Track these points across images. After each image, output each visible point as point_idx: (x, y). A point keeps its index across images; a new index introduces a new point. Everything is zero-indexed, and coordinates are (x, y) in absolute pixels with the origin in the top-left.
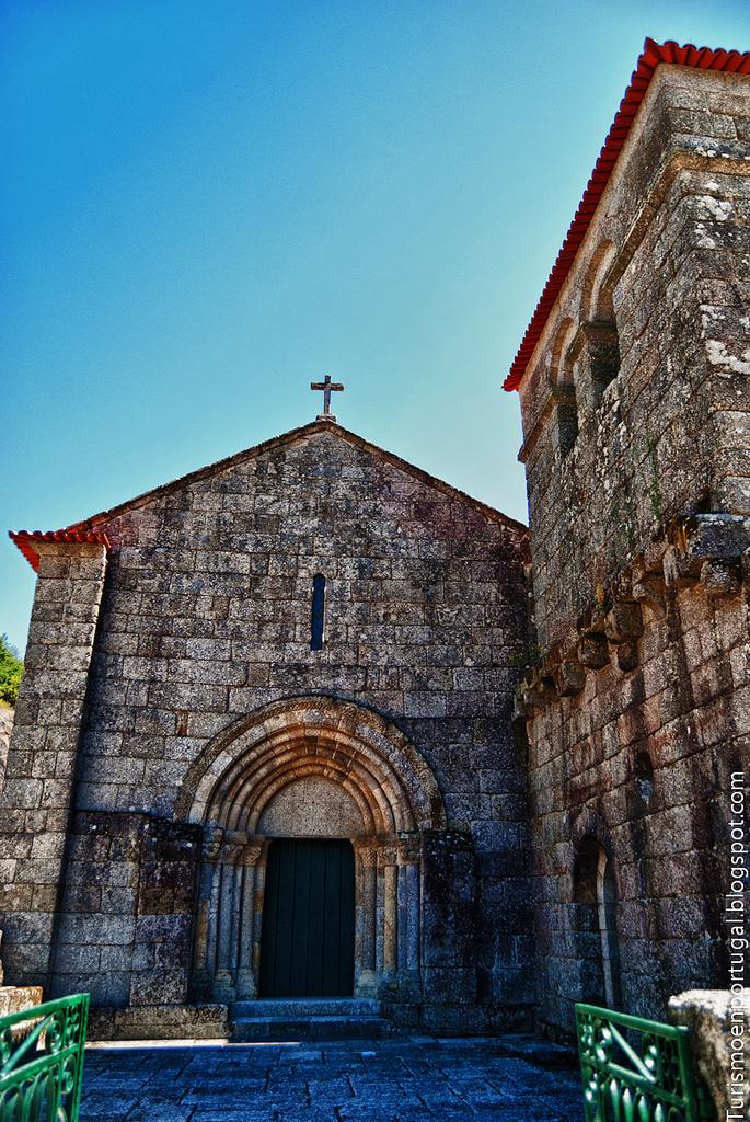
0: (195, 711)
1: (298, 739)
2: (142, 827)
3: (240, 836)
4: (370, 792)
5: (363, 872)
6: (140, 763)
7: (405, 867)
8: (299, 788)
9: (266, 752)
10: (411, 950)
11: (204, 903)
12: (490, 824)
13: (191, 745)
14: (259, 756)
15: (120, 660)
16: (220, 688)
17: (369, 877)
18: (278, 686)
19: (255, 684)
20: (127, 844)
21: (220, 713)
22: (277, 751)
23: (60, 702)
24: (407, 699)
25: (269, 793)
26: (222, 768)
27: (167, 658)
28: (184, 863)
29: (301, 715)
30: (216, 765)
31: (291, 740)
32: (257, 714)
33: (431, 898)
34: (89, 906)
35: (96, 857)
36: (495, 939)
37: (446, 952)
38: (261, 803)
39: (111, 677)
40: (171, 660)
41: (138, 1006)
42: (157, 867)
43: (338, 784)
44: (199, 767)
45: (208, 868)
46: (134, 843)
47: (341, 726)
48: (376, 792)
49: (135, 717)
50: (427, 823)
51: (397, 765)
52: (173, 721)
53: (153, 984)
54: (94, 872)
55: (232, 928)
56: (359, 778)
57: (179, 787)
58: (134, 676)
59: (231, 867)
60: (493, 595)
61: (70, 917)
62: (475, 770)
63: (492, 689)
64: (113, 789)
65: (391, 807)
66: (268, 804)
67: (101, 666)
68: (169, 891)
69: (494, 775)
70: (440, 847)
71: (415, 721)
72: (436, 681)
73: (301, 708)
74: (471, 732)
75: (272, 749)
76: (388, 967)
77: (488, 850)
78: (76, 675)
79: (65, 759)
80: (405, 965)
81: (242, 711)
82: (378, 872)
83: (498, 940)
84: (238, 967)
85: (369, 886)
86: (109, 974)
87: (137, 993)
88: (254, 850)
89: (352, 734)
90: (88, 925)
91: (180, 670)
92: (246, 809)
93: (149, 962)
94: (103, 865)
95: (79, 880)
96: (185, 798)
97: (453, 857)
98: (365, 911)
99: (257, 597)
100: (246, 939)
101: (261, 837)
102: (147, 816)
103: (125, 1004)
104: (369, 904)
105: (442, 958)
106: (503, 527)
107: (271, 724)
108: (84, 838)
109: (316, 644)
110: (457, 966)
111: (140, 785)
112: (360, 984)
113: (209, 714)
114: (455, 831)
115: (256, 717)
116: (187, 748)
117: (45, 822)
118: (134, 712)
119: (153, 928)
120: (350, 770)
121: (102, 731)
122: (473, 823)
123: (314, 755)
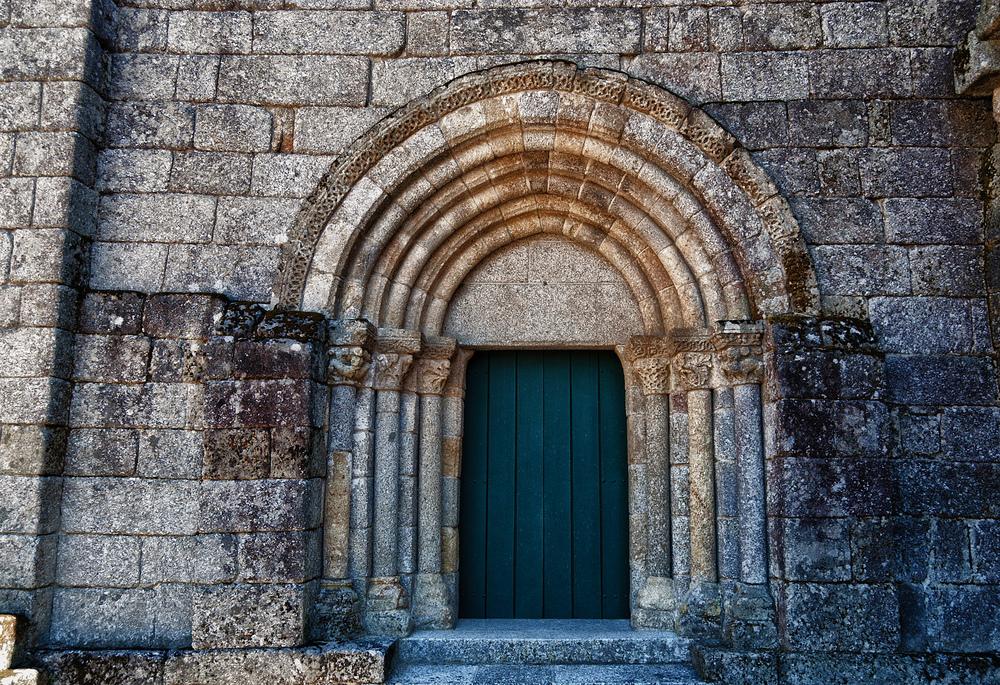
0: (308, 105)
1: (511, 155)
2: (208, 318)
3: (408, 339)
4: (654, 256)
5: (643, 404)
6: (206, 205)
8: (517, 257)
9: (448, 183)
10: (750, 546)
11: (339, 459)
12: (910, 303)
13: (303, 170)
14: (437, 191)
15: (162, 17)
16: (354, 61)
17: (655, 411)
18: (468, 53)
19: (422, 50)
20: (182, 351)
22: (472, 181)
23: (36, 85)
24: (728, 67)
25: (461, 265)
26: (363, 210)
27: (251, 10)
28: (287, 382)
29: (516, 104)
31: (495, 159)
32: (427, 104)
33: (795, 447)
34: (115, 465)
35: (125, 374)
36: (927, 525)
37: (833, 553)
38: (447, 286)
39: (145, 51)
40: (258, 14)
41: (208, 650)
42: (234, 390)
43: (590, 248)
44: (319, 210)
45: (344, 394)
46: (194, 347)
47: (596, 121)
48: (667, 255)
49: (194, 120)
50: (776, 303)
51: (711, 192)
52: (266, 126)
53: (236, 609)
56: (631, 230)
57: (281, 246)
58: (188, 45)
59: (394, 396)
61: (80, 483)
62: (873, 199)
63: (905, 41)
65: (696, 281)
66: (460, 289)
67: (127, 29)
68: (260, 436)
69: (914, 209)
70: (810, 347)
71: (747, 107)
72: (789, 30)
74: (865, 126)
75: (460, 176)
76: (700, 577)
77: (908, 353)
78: (65, 34)
79: (52, 193)
80: (738, 574)
82: (671, 402)
83: (934, 527)
84: (416, 570)
85: (655, 428)
86: (158, 588)
88: (436, 365)
89: (618, 138)
90: (115, 499)
91: (276, 31)
93: (227, 569)
94: (138, 388)
95: (96, 417)
96: (299, 269)
97: (838, 366)
98: (649, 473)
100: (428, 520)
101: (448, 342)
102: (224, 299)
103: (185, 646)
104: (656, 460)
105: (823, 564)
107: (457, 123)
110: (854, 581)
111: (207, 243)
112: (645, 602)
113: (334, 110)
114: (835, 319)
115: (421, 116)
116: (298, 173)
118: (192, 114)
119: (232, 505)
120: (614, 217)
121: (132, 147)
123: (542, 192)
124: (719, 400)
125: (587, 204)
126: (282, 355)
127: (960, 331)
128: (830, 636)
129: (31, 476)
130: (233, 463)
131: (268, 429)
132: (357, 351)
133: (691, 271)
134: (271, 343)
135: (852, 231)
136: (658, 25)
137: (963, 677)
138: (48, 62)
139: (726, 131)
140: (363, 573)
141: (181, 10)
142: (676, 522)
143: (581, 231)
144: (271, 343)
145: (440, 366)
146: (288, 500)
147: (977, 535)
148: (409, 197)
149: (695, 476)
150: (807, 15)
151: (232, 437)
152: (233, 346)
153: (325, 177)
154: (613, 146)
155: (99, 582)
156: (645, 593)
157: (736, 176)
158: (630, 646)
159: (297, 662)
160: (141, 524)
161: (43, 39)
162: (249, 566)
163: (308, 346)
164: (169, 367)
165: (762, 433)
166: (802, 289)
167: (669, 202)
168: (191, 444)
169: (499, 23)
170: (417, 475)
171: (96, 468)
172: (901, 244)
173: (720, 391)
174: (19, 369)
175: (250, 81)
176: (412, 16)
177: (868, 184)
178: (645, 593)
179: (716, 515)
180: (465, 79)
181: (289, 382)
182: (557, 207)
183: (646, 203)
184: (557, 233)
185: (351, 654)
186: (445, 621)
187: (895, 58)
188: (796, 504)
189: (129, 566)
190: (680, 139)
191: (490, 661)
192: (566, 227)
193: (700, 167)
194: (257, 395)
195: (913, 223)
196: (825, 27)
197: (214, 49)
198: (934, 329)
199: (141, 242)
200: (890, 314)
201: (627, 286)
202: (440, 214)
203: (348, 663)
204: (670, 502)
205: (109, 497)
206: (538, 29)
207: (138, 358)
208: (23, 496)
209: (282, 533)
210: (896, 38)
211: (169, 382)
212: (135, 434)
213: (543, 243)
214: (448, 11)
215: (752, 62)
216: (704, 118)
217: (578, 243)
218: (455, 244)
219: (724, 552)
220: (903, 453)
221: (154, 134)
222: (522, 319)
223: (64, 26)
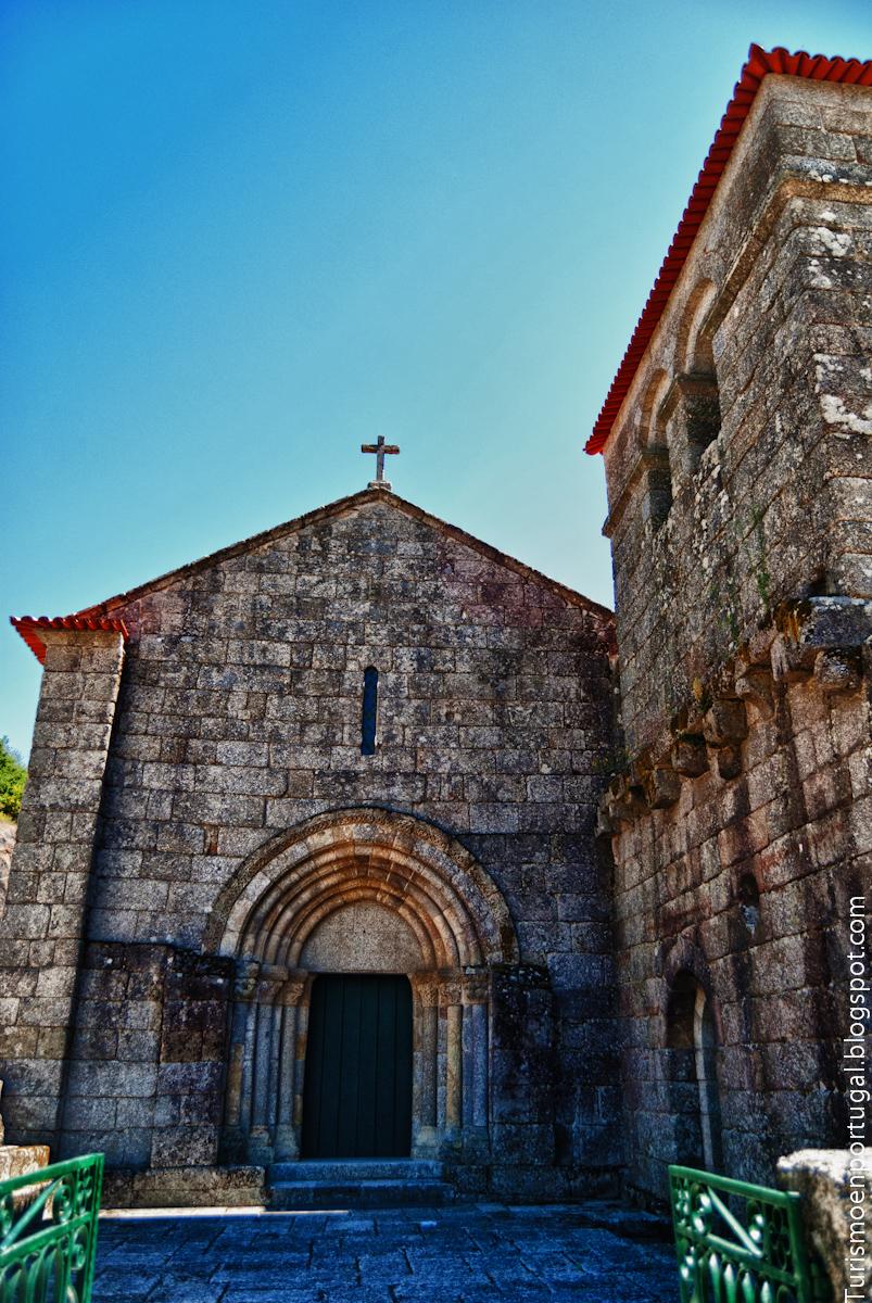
0: (227, 825)
1: (346, 858)
2: (165, 960)
3: (279, 971)
4: (430, 920)
6: (162, 887)
7: (471, 1006)
8: (348, 915)
9: (309, 874)
10: (478, 1104)
12: (570, 957)
14: (302, 878)
15: (140, 766)
16: (256, 799)
17: (429, 1018)
18: (323, 797)
20: (148, 980)
24: (473, 812)
25: (313, 921)
26: (258, 892)
27: (195, 764)
29: (350, 831)
30: (251, 888)
32: (299, 830)
34: (103, 1052)
35: (112, 995)
36: (575, 1090)
37: (519, 1106)
39: (129, 786)
40: (199, 767)
42: (182, 1007)
43: (393, 910)
44: (231, 891)
45: (242, 1007)
46: (155, 978)
47: (397, 843)
48: (438, 920)
49: (157, 833)
50: (496, 956)
51: (461, 888)
52: (201, 838)
54: (109, 1013)
55: (269, 1078)
56: (417, 903)
57: (208, 915)
58: (155, 785)
59: (269, 1007)
60: (573, 691)
61: (81, 1064)
62: (552, 894)
65: (454, 937)
68: (197, 1035)
69: (574, 900)
70: (511, 984)
71: (483, 837)
72: (508, 791)
73: (351, 823)
74: (548, 850)
75: (316, 869)
76: (452, 1122)
77: (568, 987)
78: (88, 783)
80: (471, 1121)
82: (439, 1013)
85: (429, 1029)
86: (126, 1131)
87: (159, 1153)
88: (295, 986)
89: (409, 852)
90: (102, 1075)
91: (210, 778)
93: (173, 1117)
94: (119, 1004)
95: (92, 1022)
96: (216, 927)
97: (526, 996)
99: (299, 694)
100: (286, 1090)
101: (303, 972)
102: (171, 947)
103: (146, 1166)
105: (514, 1113)
106: (585, 612)
107: (316, 841)
109: (367, 748)
110: (531, 1123)
111: (163, 911)
113: (243, 830)
116: (216, 870)
117: (52, 955)
118: (155, 828)
120: (407, 894)
121: (119, 849)
122: (550, 956)
123: (365, 877)
124: (465, 1014)
125: (392, 886)
126: (212, 986)
127: (597, 972)
128: (517, 1155)
129: (57, 1060)
130: (180, 1051)
131: (202, 1031)
132: (252, 981)
134: (205, 978)
135: (540, 913)
136: (434, 785)
137: (587, 1178)
138: (77, 800)
139: (470, 853)
140: (248, 1123)
141: (151, 762)
142: (439, 1089)
143: (386, 899)
144: (205, 978)
145: (298, 987)
146: (211, 1075)
147: (602, 1096)
148: (287, 882)
149: (450, 1061)
150: (519, 782)
151: (180, 1036)
152: (182, 979)
153: (236, 872)
154: (407, 856)
155: (89, 1127)
156: (419, 1136)
157: (475, 879)
158: (408, 1167)
159: (214, 1174)
160: (118, 1090)
161: (74, 786)
162: (187, 1115)
163: (227, 980)
164: (139, 991)
165: (487, 1034)
166: (510, 948)
167: (439, 891)
168: (151, 1039)
169: (343, 780)
170: (280, 1059)
171: (91, 1054)
172: (567, 921)
173: (466, 1007)
174: (53, 992)
175: (193, 809)
176: (292, 772)
178: (419, 1136)
179: (461, 1085)
180: (322, 816)
181: (215, 1002)
182: (373, 885)
183: (426, 889)
184: (374, 900)
185: (247, 1169)
186: (295, 1156)
187: (566, 810)
188: (500, 1077)
189: (109, 1117)
190: (444, 856)
191: (324, 1178)
192: (379, 896)
193: (455, 873)
194: (196, 1010)
195: (573, 909)
196: (529, 790)
197: (171, 788)
198: (583, 972)
199: (122, 909)
200: (559, 963)
201: (414, 934)
202: (303, 891)
203: (244, 1174)
204: (436, 1077)
205: (98, 1073)
206: (366, 785)
207: (120, 985)
208: (52, 1072)
209: (207, 1093)
210: (568, 798)
211: (139, 1000)
212: (116, 1033)
213: (364, 904)
214: (314, 771)
215: (488, 810)
216: (458, 846)
217: (385, 906)
218: (309, 908)
219: (465, 1107)
220: (564, 1047)
221: (133, 840)
222: (349, 955)
223: (88, 778)
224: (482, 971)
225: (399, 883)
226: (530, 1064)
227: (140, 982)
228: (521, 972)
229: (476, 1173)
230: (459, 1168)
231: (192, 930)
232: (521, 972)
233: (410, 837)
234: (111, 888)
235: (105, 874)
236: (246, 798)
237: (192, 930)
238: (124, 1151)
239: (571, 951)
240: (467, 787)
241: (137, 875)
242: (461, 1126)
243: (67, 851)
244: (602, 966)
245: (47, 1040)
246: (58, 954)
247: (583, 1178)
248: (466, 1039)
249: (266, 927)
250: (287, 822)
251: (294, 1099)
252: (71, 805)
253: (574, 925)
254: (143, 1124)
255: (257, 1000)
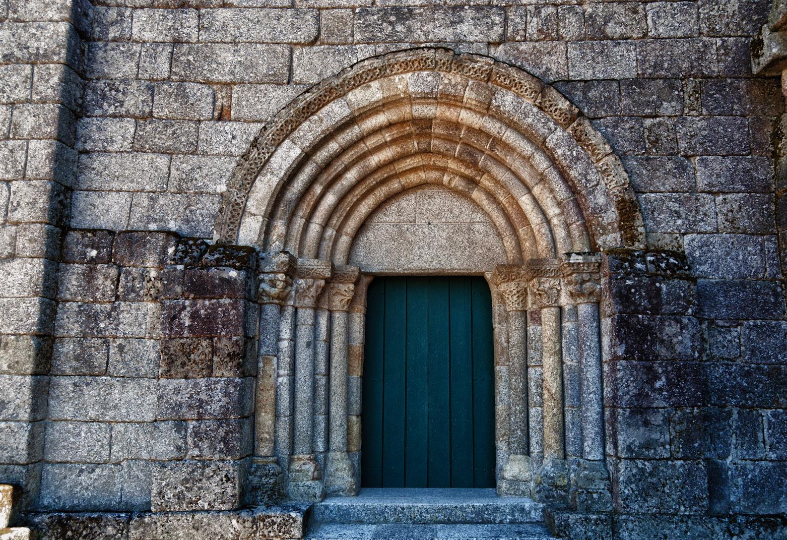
0: (242, 83)
1: (402, 122)
4: (515, 202)
5: (506, 319)
6: (162, 162)
7: (575, 308)
8: (407, 203)
9: (353, 144)
10: (591, 431)
11: (267, 362)
12: (716, 239)
13: (238, 134)
14: (344, 150)
15: (127, 13)
16: (279, 48)
17: (516, 324)
19: (332, 40)
20: (143, 277)
21: (279, 84)
22: (371, 142)
23: (28, 67)
24: (573, 53)
25: (363, 209)
26: (286, 166)
27: (197, 8)
28: (226, 301)
30: (276, 161)
31: (390, 125)
32: (336, 82)
33: (626, 352)
34: (91, 366)
35: (98, 295)
36: (730, 414)
37: (656, 436)
38: (351, 225)
39: (114, 40)
40: (203, 11)
41: (164, 512)
42: (184, 308)
43: (464, 195)
45: (271, 311)
46: (153, 274)
47: (469, 95)
48: (525, 201)
49: (153, 95)
50: (612, 239)
51: (560, 152)
52: (210, 100)
53: (186, 481)
54: (95, 317)
55: (314, 397)
56: (497, 182)
57: (222, 194)
58: (148, 36)
59: (310, 312)
61: (63, 381)
63: (713, 33)
64: (124, 198)
65: (548, 222)
66: (363, 227)
67: (100, 23)
68: (204, 343)
69: (718, 164)
72: (621, 24)
73: (405, 71)
74: (681, 99)
75: (362, 139)
76: (551, 455)
77: (715, 279)
78: (51, 27)
80: (581, 452)
81: (315, 80)
82: (528, 317)
83: (735, 416)
84: (327, 449)
85: (516, 337)
86: (124, 464)
87: (161, 493)
89: (487, 109)
90: (90, 393)
91: (218, 25)
92: (330, 232)
93: (178, 448)
94: (109, 306)
95: (75, 329)
97: (660, 289)
98: (510, 373)
100: (337, 410)
101: (352, 270)
102: (177, 237)
103: (146, 510)
104: (517, 363)
107: (360, 97)
108: (79, 268)
110: (672, 458)
111: (163, 192)
112: (508, 475)
113: (263, 87)
114: (658, 251)
117: (13, 244)
118: (151, 89)
119: (183, 398)
120: (484, 171)
121: (104, 116)
122: (687, 238)
123: (426, 152)
124: (566, 315)
126: (222, 280)
128: (653, 501)
129: (24, 375)
130: (183, 365)
131: (211, 339)
132: (281, 276)
133: (544, 213)
135: (671, 182)
136: (518, 20)
137: (758, 534)
138: (38, 49)
139: (572, 103)
141: (142, 8)
142: (533, 411)
143: (457, 182)
144: (213, 271)
145: (346, 289)
146: (227, 394)
147: (769, 422)
148: (322, 155)
149: (547, 376)
151: (183, 345)
152: (184, 272)
153: (256, 139)
154: (483, 115)
155: (78, 458)
156: (508, 467)
157: (579, 139)
158: (496, 509)
159: (234, 522)
160: (111, 414)
161: (34, 31)
165: (600, 342)
166: (631, 227)
167: (527, 159)
168: (150, 350)
169: (393, 18)
170: (328, 374)
171: (75, 369)
172: (709, 193)
173: (567, 308)
176: (324, 12)
177: (683, 145)
178: (508, 467)
179: (563, 406)
180: (366, 63)
182: (438, 164)
183: (508, 160)
184: (438, 184)
185: (276, 515)
186: (350, 490)
187: (705, 46)
188: (627, 398)
189: (102, 447)
190: (535, 110)
192: (446, 179)
193: (551, 131)
194: (202, 311)
195: (718, 176)
199: (111, 191)
200: (700, 248)
201: (494, 226)
202: (347, 169)
203: (274, 523)
204: (527, 395)
206: (423, 23)
207: (108, 282)
208: (18, 391)
209: (222, 420)
210: (705, 30)
211: (133, 301)
212: (106, 342)
213: (428, 191)
214: (353, 8)
216: (554, 93)
218: (358, 192)
219: (570, 435)
220: (711, 357)
221: (122, 106)
223: (51, 20)
224: (593, 259)
225: (472, 156)
226: (667, 378)
227: (134, 279)
228: (649, 258)
229: (597, 525)
230: (572, 518)
231: (202, 215)
232: (649, 258)
233: (487, 88)
234: (96, 165)
235: (88, 148)
236: (264, 47)
237: (202, 215)
238: (122, 489)
239: (718, 232)
240: (564, 21)
241: (128, 149)
242: (565, 458)
243: (26, 113)
244: (761, 250)
245: (10, 351)
246: (21, 243)
247: (753, 534)
248: (569, 349)
249: (301, 213)
250: (320, 75)
251: (348, 421)
252: (31, 54)
253: (721, 197)
254: (145, 455)
255: (292, 303)
